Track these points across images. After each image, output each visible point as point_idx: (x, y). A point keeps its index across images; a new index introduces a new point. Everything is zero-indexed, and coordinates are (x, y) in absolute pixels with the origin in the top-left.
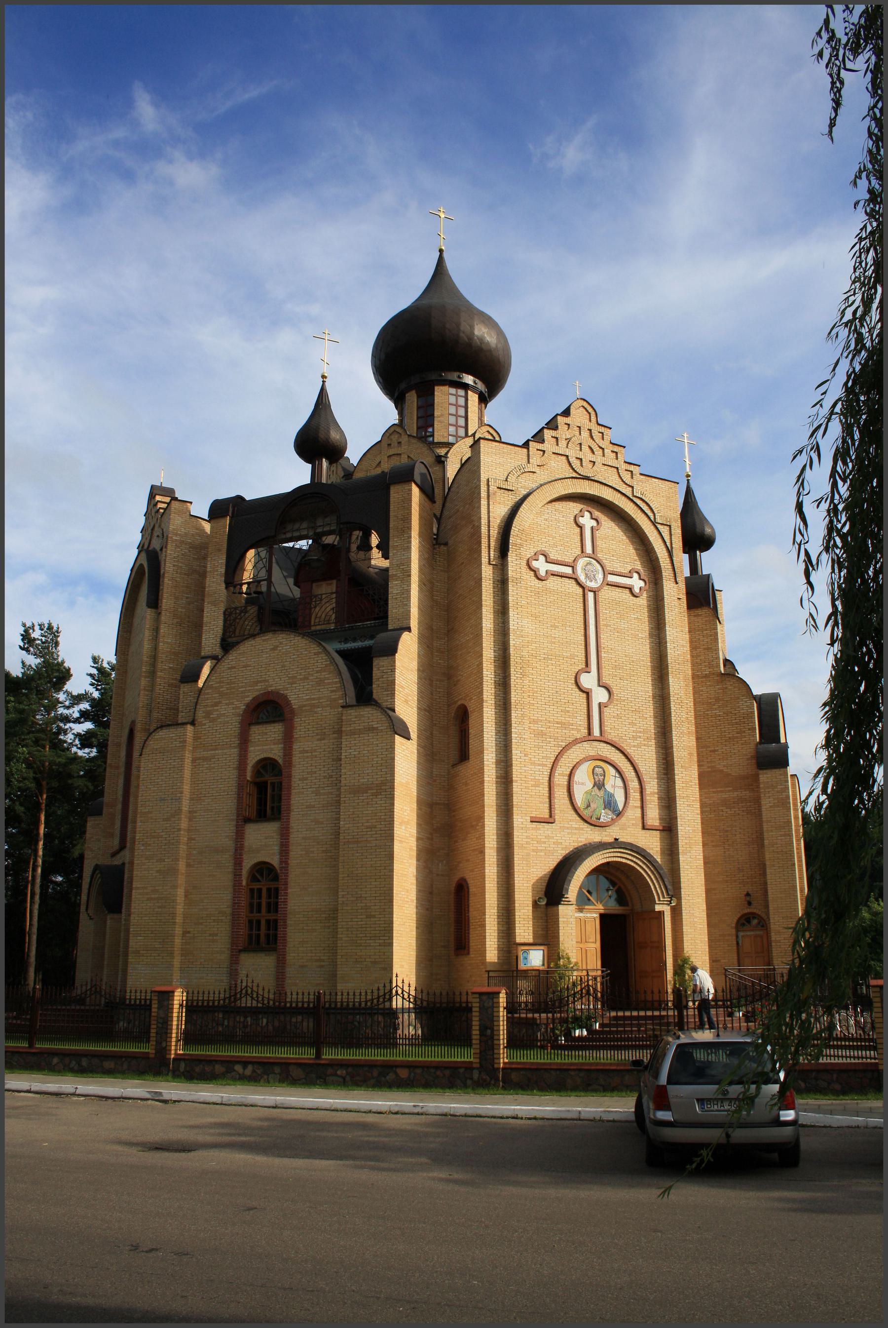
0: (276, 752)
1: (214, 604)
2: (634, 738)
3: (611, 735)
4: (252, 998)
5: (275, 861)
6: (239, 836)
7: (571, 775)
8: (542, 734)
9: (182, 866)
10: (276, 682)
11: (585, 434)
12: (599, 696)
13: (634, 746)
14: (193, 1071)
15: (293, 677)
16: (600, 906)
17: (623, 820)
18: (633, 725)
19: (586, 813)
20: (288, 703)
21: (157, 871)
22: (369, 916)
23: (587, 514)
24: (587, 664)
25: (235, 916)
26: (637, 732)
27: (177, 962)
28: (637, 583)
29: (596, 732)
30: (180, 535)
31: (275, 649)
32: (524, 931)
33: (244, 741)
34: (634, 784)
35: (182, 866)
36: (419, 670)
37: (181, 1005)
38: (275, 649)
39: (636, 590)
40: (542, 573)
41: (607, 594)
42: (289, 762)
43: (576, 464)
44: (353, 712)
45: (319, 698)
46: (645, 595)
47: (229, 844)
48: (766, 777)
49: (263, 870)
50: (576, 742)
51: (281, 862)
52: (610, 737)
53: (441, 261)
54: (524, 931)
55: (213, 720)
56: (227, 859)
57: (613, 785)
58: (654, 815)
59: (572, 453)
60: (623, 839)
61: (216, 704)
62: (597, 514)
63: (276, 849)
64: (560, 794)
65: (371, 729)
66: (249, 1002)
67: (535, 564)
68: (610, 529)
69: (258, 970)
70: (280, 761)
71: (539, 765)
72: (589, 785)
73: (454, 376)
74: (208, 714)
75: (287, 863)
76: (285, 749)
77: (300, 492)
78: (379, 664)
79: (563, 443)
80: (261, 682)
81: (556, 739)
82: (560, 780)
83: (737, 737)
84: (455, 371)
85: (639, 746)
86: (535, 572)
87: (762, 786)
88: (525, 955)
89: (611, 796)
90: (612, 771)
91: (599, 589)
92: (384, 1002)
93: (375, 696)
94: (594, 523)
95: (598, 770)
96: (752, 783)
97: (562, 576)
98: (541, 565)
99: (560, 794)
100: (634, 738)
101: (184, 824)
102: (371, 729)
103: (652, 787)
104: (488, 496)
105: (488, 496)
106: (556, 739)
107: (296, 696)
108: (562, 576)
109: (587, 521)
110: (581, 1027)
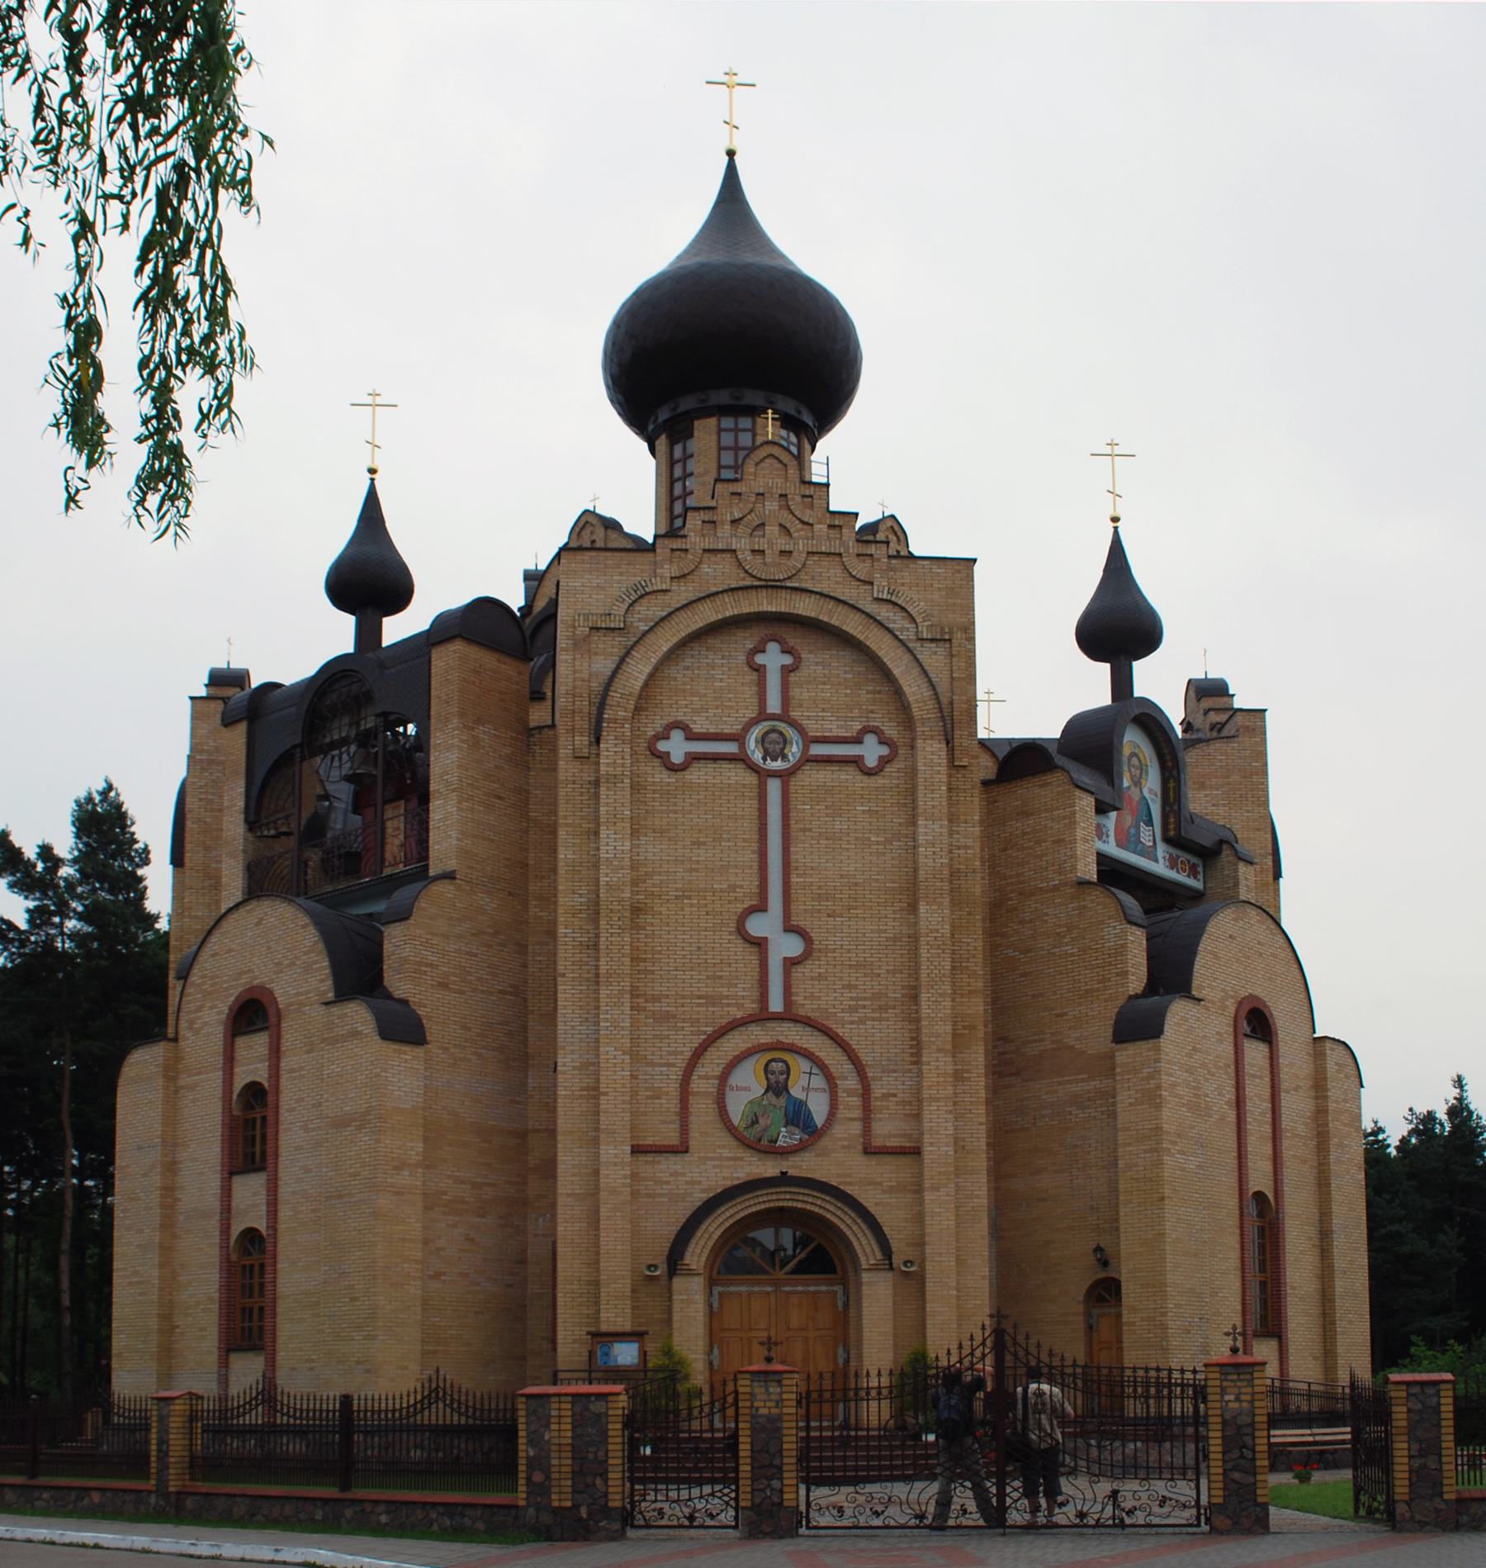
0: (262, 1075)
2: (853, 1009)
3: (806, 1007)
4: (460, 1414)
5: (262, 1226)
6: (227, 1193)
7: (724, 1077)
10: (262, 974)
11: (772, 506)
12: (786, 946)
13: (852, 1023)
15: (279, 964)
17: (825, 1142)
19: (750, 1135)
21: (138, 1246)
22: (353, 1299)
26: (857, 999)
29: (776, 1005)
30: (206, 751)
34: (849, 1082)
40: (677, 758)
44: (336, 1010)
45: (307, 992)
47: (213, 1203)
48: (1128, 1054)
49: (251, 1237)
52: (801, 1012)
55: (196, 1032)
56: (214, 1224)
59: (742, 544)
60: (791, 1172)
61: (199, 1009)
64: (702, 1110)
65: (355, 1034)
66: (456, 1418)
67: (662, 746)
69: (247, 1371)
70: (266, 1085)
71: (662, 1065)
72: (758, 1089)
74: (191, 1022)
77: (335, 672)
80: (245, 973)
81: (694, 1022)
83: (1098, 990)
85: (861, 1021)
86: (664, 758)
87: (1118, 1070)
88: (605, 1349)
92: (408, 1418)
94: (788, 660)
98: (677, 747)
100: (853, 1009)
102: (355, 1034)
106: (694, 1022)
107: (284, 991)
109: (773, 659)
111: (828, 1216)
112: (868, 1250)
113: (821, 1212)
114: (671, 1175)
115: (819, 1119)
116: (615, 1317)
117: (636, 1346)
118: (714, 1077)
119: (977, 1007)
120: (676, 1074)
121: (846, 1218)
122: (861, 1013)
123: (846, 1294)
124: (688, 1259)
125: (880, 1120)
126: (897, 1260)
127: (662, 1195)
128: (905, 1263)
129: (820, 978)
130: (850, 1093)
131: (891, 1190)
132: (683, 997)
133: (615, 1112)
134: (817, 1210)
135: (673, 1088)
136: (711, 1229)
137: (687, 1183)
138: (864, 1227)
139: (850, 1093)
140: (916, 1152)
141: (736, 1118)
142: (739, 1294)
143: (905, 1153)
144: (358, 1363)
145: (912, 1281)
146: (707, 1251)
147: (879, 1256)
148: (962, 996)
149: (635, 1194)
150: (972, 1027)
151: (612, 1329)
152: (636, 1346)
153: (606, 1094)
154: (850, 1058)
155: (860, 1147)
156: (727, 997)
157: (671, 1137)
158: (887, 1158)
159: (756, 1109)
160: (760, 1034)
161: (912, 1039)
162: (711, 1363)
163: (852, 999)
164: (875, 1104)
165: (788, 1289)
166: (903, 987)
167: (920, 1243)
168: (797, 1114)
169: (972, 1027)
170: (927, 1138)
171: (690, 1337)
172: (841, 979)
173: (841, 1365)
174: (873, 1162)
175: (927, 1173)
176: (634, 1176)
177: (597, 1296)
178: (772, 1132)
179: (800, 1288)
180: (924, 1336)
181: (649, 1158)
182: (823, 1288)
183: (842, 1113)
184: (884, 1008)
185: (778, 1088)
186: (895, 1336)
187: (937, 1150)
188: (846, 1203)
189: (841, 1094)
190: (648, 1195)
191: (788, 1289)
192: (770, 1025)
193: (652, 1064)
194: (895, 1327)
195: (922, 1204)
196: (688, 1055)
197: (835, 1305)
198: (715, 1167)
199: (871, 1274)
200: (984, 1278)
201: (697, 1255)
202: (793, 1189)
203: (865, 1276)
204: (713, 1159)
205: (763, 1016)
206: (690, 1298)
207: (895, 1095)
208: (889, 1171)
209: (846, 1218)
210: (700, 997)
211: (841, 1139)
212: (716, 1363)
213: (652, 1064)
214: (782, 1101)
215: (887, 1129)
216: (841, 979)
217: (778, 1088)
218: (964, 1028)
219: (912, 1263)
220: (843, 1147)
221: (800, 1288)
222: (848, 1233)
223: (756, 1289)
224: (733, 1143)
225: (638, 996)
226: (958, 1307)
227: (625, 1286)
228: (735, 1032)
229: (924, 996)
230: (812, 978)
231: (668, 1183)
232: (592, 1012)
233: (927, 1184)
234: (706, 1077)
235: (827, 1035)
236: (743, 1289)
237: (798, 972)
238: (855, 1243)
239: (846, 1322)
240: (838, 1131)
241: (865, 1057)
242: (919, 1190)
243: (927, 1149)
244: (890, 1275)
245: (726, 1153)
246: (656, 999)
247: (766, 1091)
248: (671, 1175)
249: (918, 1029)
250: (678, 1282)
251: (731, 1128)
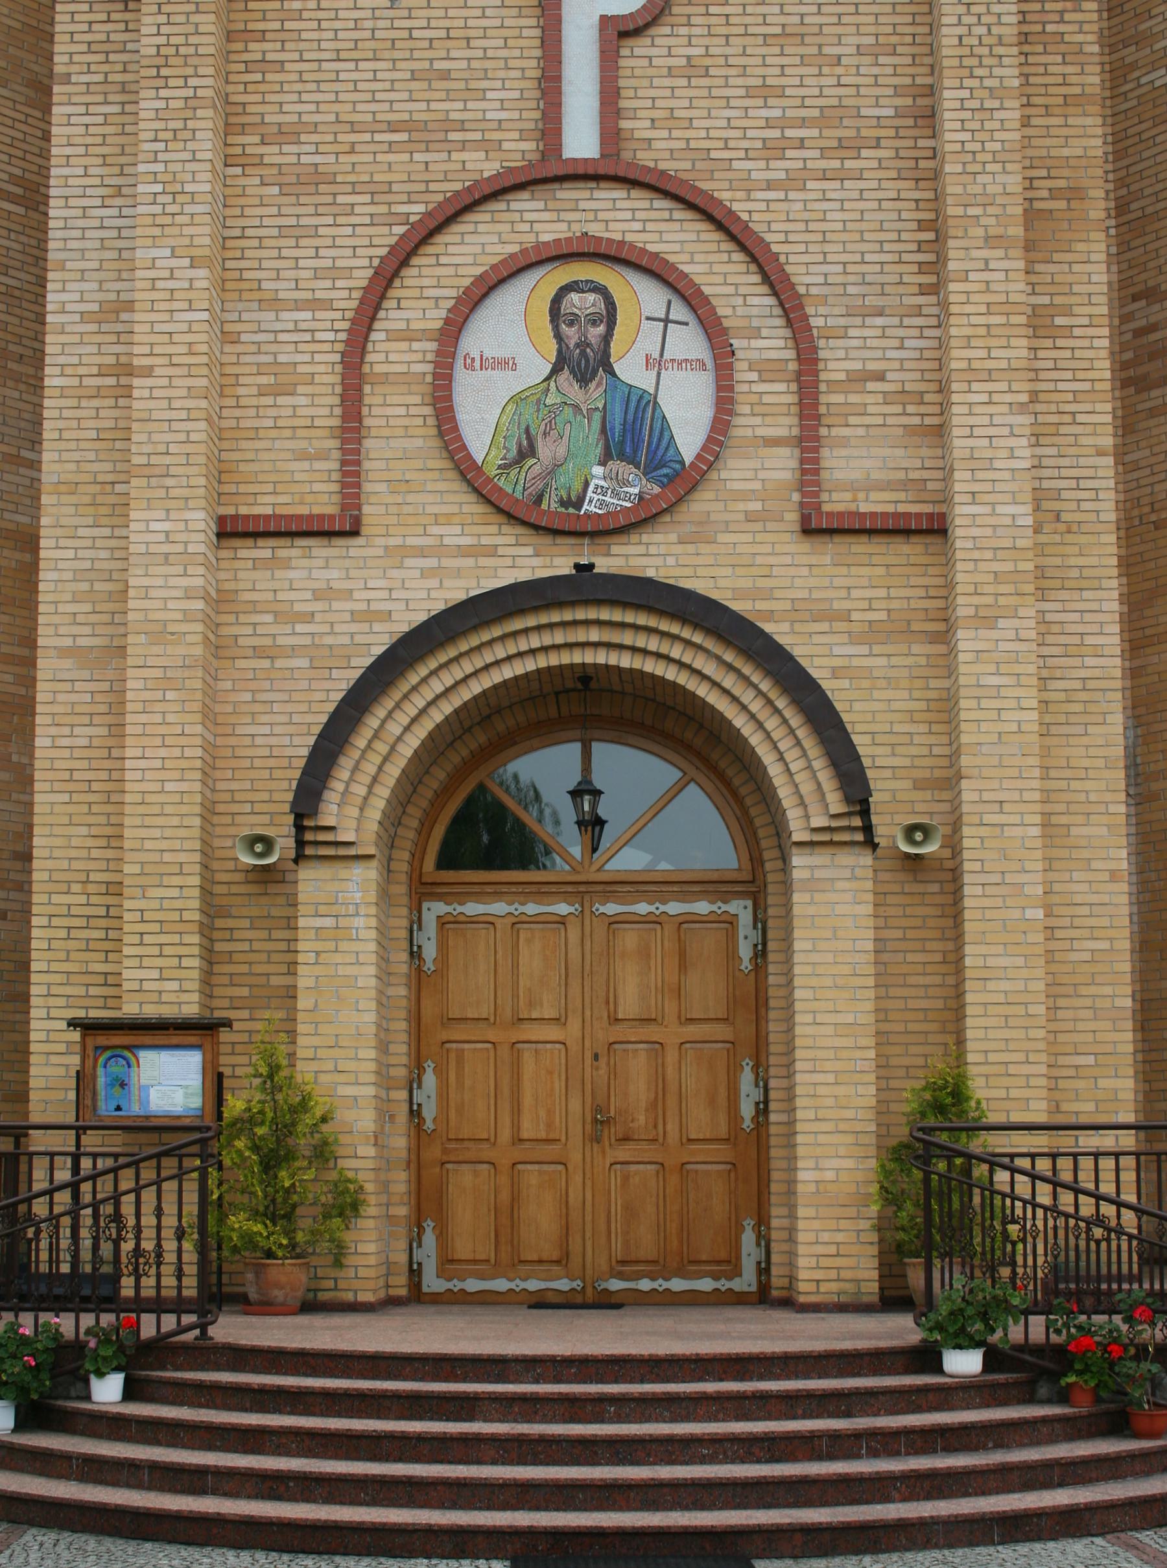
2: (773, 151)
3: (656, 148)
7: (452, 331)
13: (770, 186)
17: (702, 503)
19: (513, 485)
26: (782, 123)
29: (581, 141)
34: (765, 343)
52: (645, 158)
71: (298, 305)
72: (535, 366)
81: (378, 191)
85: (795, 181)
88: (117, 1068)
111: (702, 690)
112: (806, 788)
113: (682, 679)
114: (317, 595)
115: (688, 441)
116: (161, 982)
117: (194, 1059)
118: (424, 335)
119: (1086, 139)
120: (331, 328)
121: (747, 697)
122: (793, 160)
123: (760, 921)
124: (330, 812)
125: (844, 442)
126: (887, 828)
127: (294, 651)
128: (910, 831)
129: (692, 69)
130: (766, 371)
131: (872, 634)
132: (353, 128)
133: (170, 418)
134: (670, 673)
135: (325, 366)
136: (395, 729)
137: (355, 617)
138: (795, 721)
139: (766, 371)
140: (934, 529)
141: (479, 440)
142: (489, 922)
143: (907, 532)
145: (928, 878)
146: (384, 792)
147: (836, 803)
148: (1047, 110)
149: (219, 649)
150: (1075, 194)
151: (151, 1011)
152: (194, 1059)
153: (148, 372)
154: (766, 279)
155: (793, 517)
156: (462, 126)
157: (320, 497)
158: (860, 547)
159: (529, 414)
160: (539, 220)
161: (922, 226)
162: (415, 1113)
163: (769, 124)
164: (829, 398)
165: (611, 909)
166: (898, 91)
167: (948, 780)
168: (632, 428)
169: (1075, 194)
170: (962, 482)
171: (341, 1032)
172: (744, 72)
173: (747, 1124)
174: (828, 551)
175: (963, 576)
176: (221, 602)
177: (113, 916)
178: (567, 481)
179: (643, 908)
180: (961, 1042)
181: (263, 550)
182: (702, 907)
183: (745, 425)
184: (848, 147)
185: (583, 362)
186: (882, 1039)
187: (990, 517)
188: (747, 653)
189: (743, 374)
190: (258, 652)
191: (611, 909)
192: (567, 193)
193: (274, 304)
194: (882, 1014)
195: (949, 667)
196: (362, 277)
197: (732, 954)
198: (425, 573)
199: (819, 858)
200: (1114, 876)
201: (357, 806)
202: (605, 614)
203: (799, 861)
204: (421, 552)
205: (549, 175)
206: (345, 921)
207: (880, 377)
208: (867, 581)
209: (747, 697)
210: (393, 128)
211: (744, 496)
212: (429, 1113)
213: (274, 304)
214: (595, 395)
215: (864, 468)
216: (744, 72)
217: (583, 362)
218: (1054, 194)
219: (925, 830)
220: (750, 517)
221: (643, 908)
222: (755, 740)
223: (531, 909)
224: (473, 507)
225: (243, 129)
226: (1050, 956)
227: (181, 895)
228: (479, 216)
229: (950, 97)
230: (671, 72)
231: (310, 617)
232: (120, 160)
233: (964, 607)
234: (407, 336)
235: (709, 218)
236: (499, 908)
237: (637, 55)
238: (774, 770)
239: (759, 1003)
240: (737, 473)
241: (805, 276)
242: (943, 632)
243: (963, 514)
244: (866, 859)
245: (454, 536)
246: (287, 134)
247: (556, 370)
248: (317, 595)
249: (938, 198)
250: (312, 882)
251: (466, 470)
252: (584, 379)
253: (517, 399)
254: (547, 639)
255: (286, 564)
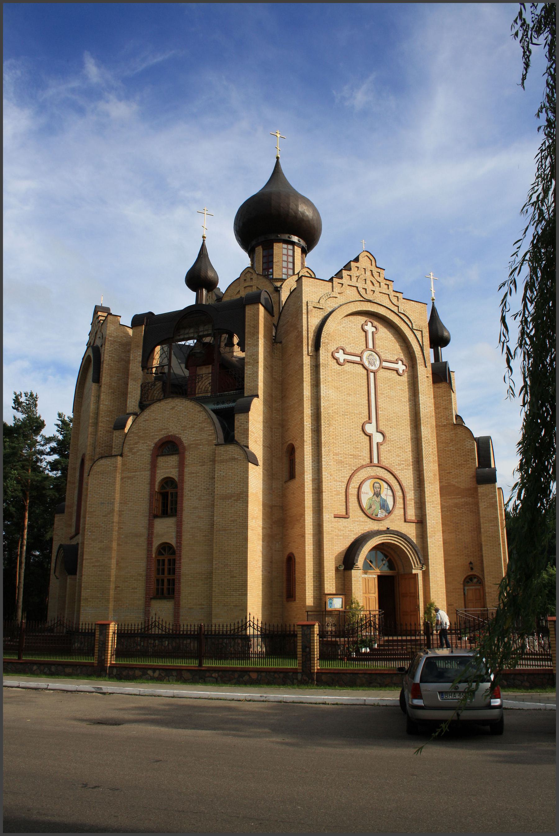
0: (173, 473)
1: (135, 380)
2: (399, 465)
3: (385, 463)
4: (159, 628)
5: (173, 542)
6: (151, 526)
7: (359, 488)
8: (341, 462)
9: (114, 545)
10: (174, 429)
11: (368, 273)
12: (377, 438)
13: (399, 470)
14: (122, 674)
15: (185, 426)
16: (378, 571)
17: (392, 516)
18: (399, 457)
19: (369, 512)
20: (181, 442)
21: (99, 549)
22: (232, 577)
23: (369, 324)
24: (370, 418)
25: (148, 577)
26: (401, 461)
27: (111, 605)
28: (401, 367)
29: (375, 461)
30: (113, 337)
31: (173, 408)
32: (330, 586)
33: (154, 466)
34: (399, 494)
35: (114, 545)
36: (263, 422)
37: (114, 633)
38: (173, 408)
39: (401, 372)
40: (341, 361)
41: (382, 374)
42: (182, 480)
43: (362, 292)
44: (222, 448)
45: (201, 440)
46: (406, 374)
47: (144, 531)
48: (482, 489)
49: (165, 548)
50: (362, 467)
51: (177, 543)
52: (384, 464)
53: (277, 165)
54: (330, 586)
55: (134, 453)
56: (143, 541)
57: (386, 494)
58: (412, 513)
59: (360, 285)
60: (392, 528)
61: (136, 443)
62: (376, 323)
63: (174, 534)
64: (353, 500)
65: (234, 459)
66: (157, 631)
67: (337, 355)
68: (384, 333)
69: (162, 610)
70: (176, 479)
71: (339, 482)
72: (371, 494)
73: (286, 237)
74: (131, 450)
75: (180, 543)
76: (179, 471)
77: (189, 310)
78: (239, 418)
79: (354, 279)
80: (164, 429)
81: (350, 465)
82: (353, 491)
83: (464, 464)
84: (287, 233)
85: (402, 470)
86: (337, 360)
87: (479, 495)
88: (331, 601)
89: (385, 501)
90: (385, 485)
91: (377, 371)
93: (236, 438)
94: (374, 329)
95: (376, 485)
96: (473, 493)
97: (354, 363)
98: (341, 356)
99: (353, 500)
100: (399, 465)
101: (116, 519)
102: (234, 459)
103: (411, 495)
104: (307, 312)
105: (307, 312)
106: (350, 465)
107: (186, 438)
108: (354, 363)
109: (369, 328)
110: (366, 647)
144: (236, 606)
252: (377, 497)
253: (369, 499)
254: (401, 542)
255: (339, 522)
